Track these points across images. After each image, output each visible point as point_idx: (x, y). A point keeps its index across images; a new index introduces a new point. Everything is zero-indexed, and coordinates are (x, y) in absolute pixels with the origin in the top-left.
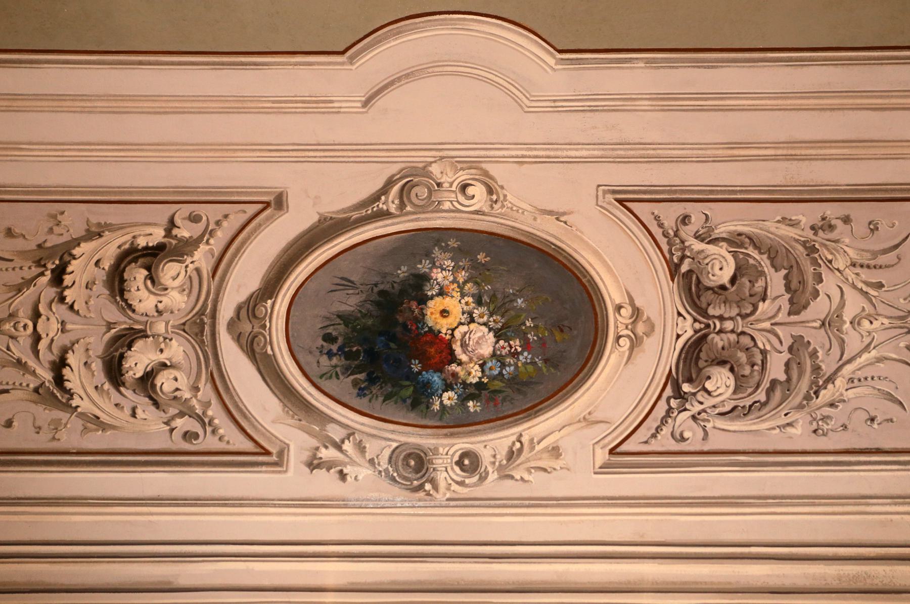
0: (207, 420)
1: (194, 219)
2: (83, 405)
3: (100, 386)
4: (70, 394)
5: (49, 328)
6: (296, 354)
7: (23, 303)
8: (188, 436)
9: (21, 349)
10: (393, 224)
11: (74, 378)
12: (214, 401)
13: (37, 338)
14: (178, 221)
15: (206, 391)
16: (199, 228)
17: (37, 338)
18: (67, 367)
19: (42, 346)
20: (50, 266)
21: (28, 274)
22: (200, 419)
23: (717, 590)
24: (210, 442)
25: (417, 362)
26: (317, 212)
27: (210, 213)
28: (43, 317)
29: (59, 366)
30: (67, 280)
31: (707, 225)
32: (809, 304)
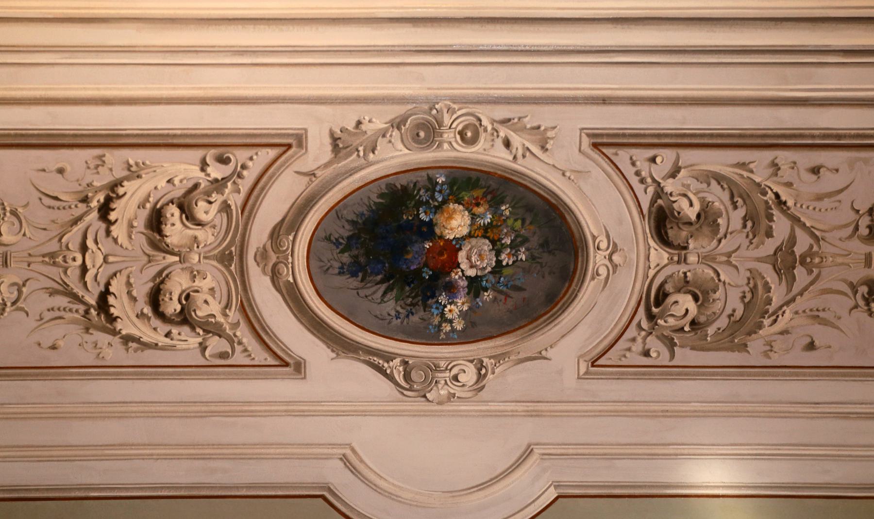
0: (236, 340)
1: (223, 160)
2: (126, 327)
3: (542, 128)
4: (112, 319)
5: (95, 259)
6: (315, 280)
7: (73, 237)
8: (223, 355)
9: (72, 279)
10: (804, 450)
11: (118, 305)
12: (243, 324)
13: (84, 269)
14: (208, 160)
15: (234, 314)
16: (226, 170)
17: (84, 269)
18: (112, 295)
19: (89, 277)
20: (94, 204)
21: (77, 212)
22: (231, 341)
23: (283, 21)
24: (239, 358)
25: (424, 275)
26: (780, 285)
27: (239, 156)
28: (90, 251)
29: (105, 294)
30: (112, 216)
31: (8, 214)
32: (771, 227)
